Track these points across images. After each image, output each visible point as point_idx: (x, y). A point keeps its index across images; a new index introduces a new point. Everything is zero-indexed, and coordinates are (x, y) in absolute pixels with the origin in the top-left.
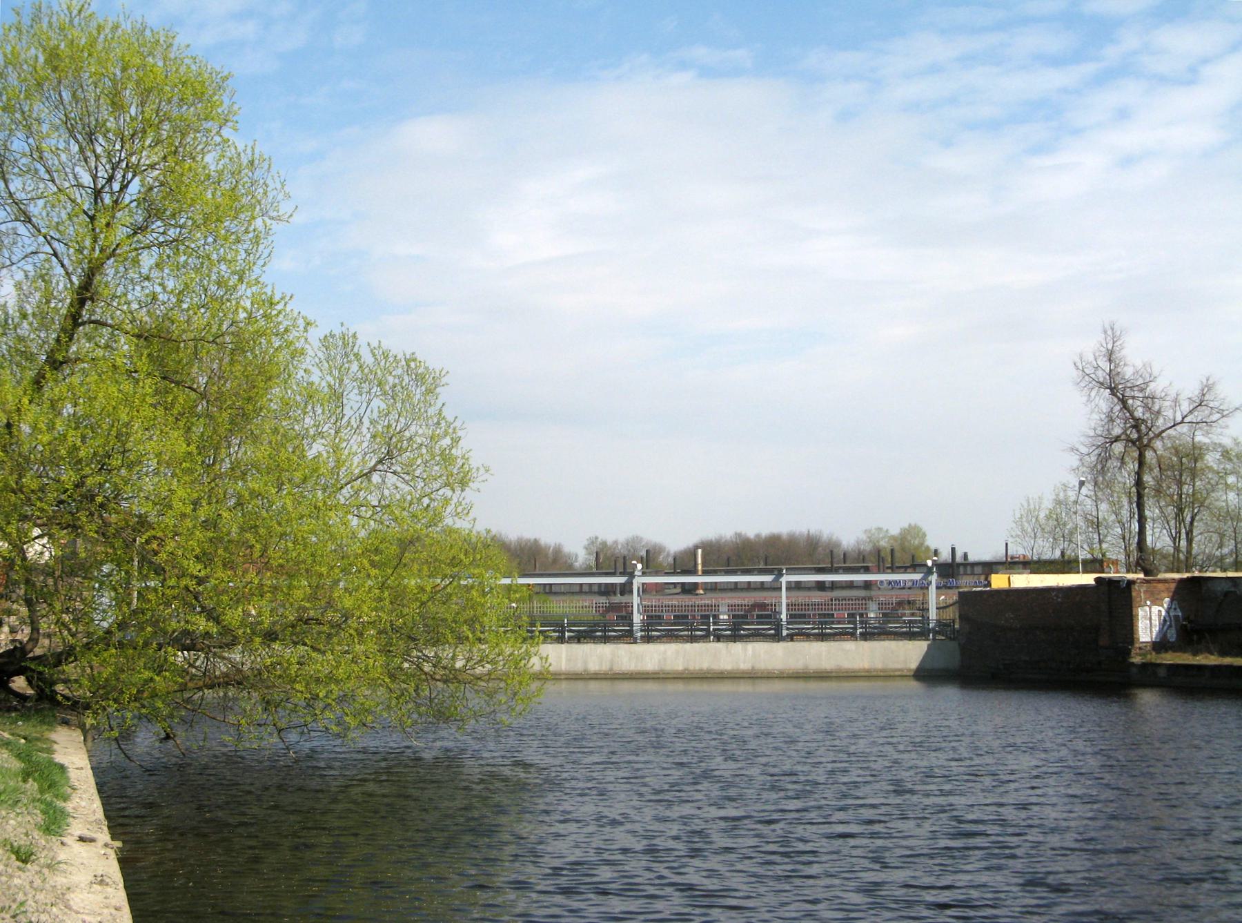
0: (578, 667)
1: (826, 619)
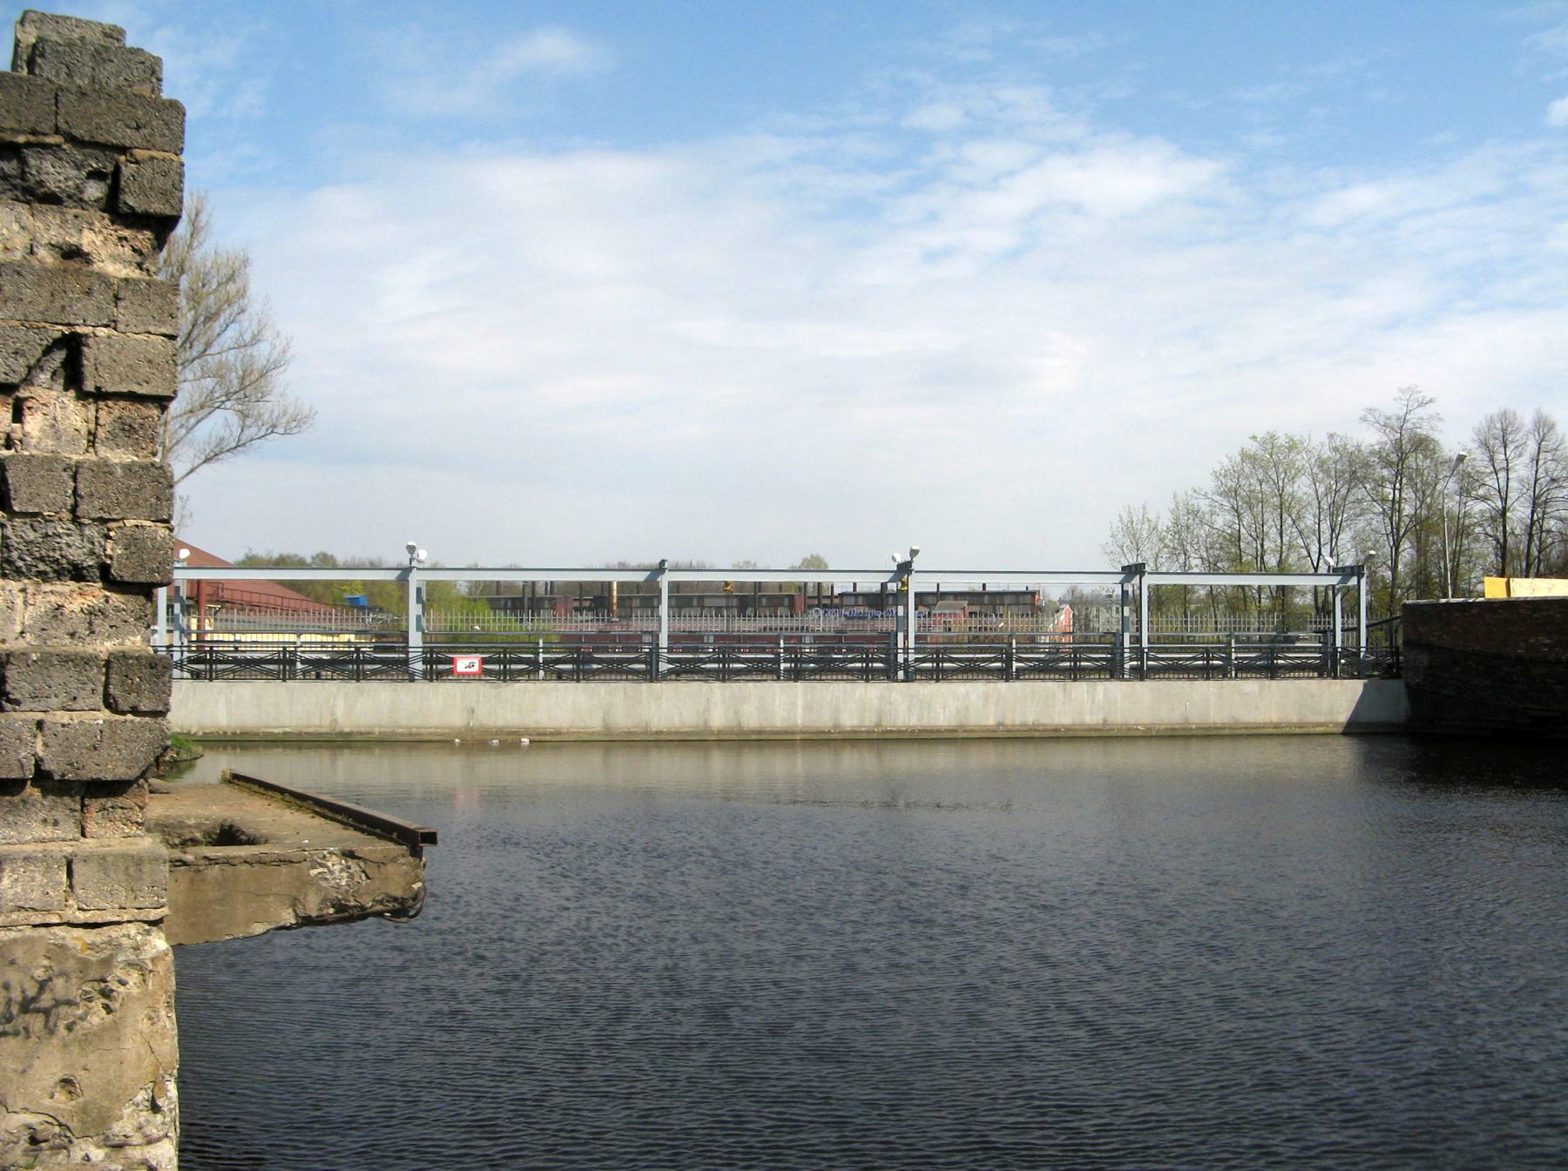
0: (824, 721)
1: (728, 645)
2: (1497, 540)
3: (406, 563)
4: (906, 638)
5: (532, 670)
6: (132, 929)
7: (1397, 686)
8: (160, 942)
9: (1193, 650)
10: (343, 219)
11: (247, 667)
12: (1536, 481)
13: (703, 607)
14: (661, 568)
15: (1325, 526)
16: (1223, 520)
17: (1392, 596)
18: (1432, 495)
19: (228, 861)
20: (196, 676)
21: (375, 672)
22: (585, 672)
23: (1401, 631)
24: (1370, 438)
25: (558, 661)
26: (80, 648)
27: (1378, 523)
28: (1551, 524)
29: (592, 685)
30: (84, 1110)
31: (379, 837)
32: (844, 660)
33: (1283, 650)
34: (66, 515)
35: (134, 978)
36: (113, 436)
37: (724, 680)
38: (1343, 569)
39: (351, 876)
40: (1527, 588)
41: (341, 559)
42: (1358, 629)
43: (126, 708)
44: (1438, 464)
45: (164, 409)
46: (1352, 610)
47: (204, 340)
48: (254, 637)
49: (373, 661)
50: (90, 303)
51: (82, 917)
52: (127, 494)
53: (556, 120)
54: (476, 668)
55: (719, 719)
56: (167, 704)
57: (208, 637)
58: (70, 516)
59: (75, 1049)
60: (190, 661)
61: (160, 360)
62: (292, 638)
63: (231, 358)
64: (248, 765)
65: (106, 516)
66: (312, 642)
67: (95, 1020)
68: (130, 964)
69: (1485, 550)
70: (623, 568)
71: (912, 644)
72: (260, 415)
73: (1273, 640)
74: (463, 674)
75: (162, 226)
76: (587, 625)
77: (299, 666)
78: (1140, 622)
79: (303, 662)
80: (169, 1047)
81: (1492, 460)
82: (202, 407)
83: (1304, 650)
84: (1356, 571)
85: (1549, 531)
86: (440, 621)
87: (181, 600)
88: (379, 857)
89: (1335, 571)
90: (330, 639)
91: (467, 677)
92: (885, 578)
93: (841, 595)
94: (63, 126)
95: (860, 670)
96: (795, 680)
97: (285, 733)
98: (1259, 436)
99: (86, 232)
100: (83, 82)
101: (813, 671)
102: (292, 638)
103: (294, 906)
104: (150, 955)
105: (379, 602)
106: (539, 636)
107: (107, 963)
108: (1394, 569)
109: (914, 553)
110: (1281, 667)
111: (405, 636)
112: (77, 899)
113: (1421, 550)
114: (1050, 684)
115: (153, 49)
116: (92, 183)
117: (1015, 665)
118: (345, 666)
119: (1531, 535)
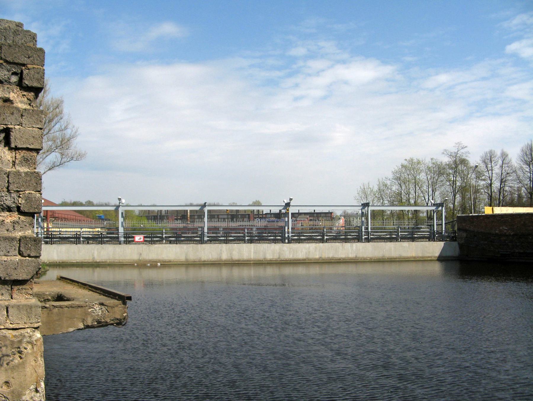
0: (260, 257)
1: (228, 231)
2: (489, 194)
3: (118, 204)
4: (288, 228)
5: (161, 240)
6: (29, 330)
7: (455, 244)
8: (38, 335)
9: (385, 232)
10: (97, 86)
11: (64, 240)
12: (502, 174)
13: (219, 218)
14: (204, 205)
15: (430, 189)
16: (395, 188)
17: (453, 213)
18: (467, 179)
19: (61, 307)
20: (46, 243)
21: (107, 241)
22: (179, 241)
23: (456, 225)
24: (446, 160)
25: (170, 237)
26: (10, 235)
27: (447, 188)
28: (507, 188)
29: (182, 245)
30: (13, 392)
31: (112, 298)
32: (267, 236)
33: (416, 232)
34: (5, 190)
35: (29, 347)
36: (21, 162)
37: (226, 243)
38: (437, 204)
39: (102, 312)
40: (499, 210)
41: (95, 202)
42: (442, 225)
43: (26, 255)
44: (469, 168)
45: (38, 153)
46: (440, 218)
47: (48, 128)
48: (66, 230)
49: (107, 237)
50: (13, 117)
51: (11, 326)
52: (26, 182)
53: (168, 53)
54: (142, 240)
55: (225, 256)
56: (40, 254)
57: (50, 230)
58: (6, 190)
59: (10, 371)
60: (44, 238)
61: (37, 136)
62: (79, 230)
63: (58, 135)
64: (65, 273)
65: (19, 190)
66: (86, 231)
67: (16, 361)
68: (28, 342)
69: (485, 197)
70: (191, 205)
71: (290, 230)
72: (68, 154)
73: (413, 228)
74: (138, 242)
75: (37, 91)
76: (180, 224)
77: (82, 239)
78: (368, 222)
79: (83, 238)
80: (41, 371)
81: (487, 167)
82: (48, 151)
83: (424, 232)
84: (441, 205)
85: (506, 191)
86: (129, 224)
87: (41, 217)
88: (112, 305)
89: (434, 205)
90: (92, 230)
91: (139, 243)
92: (281, 208)
93: (266, 214)
94: (3, 57)
95: (273, 240)
96: (251, 243)
97: (77, 262)
98: (408, 159)
99: (11, 93)
100: (10, 42)
101: (257, 240)
102: (79, 230)
103: (83, 322)
104: (35, 339)
105: (108, 217)
106: (163, 228)
107: (20, 342)
108: (454, 204)
109: (291, 199)
110: (416, 237)
111: (117, 229)
112: (10, 320)
113: (463, 198)
114: (337, 244)
115: (34, 31)
116: (13, 76)
117: (325, 237)
118: (97, 239)
119: (500, 192)
